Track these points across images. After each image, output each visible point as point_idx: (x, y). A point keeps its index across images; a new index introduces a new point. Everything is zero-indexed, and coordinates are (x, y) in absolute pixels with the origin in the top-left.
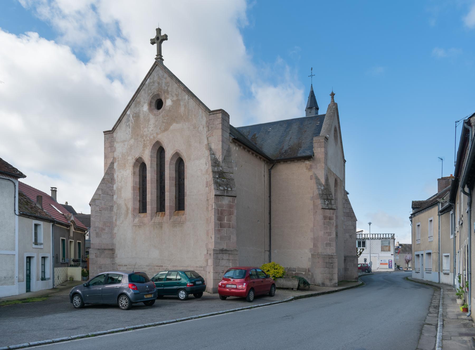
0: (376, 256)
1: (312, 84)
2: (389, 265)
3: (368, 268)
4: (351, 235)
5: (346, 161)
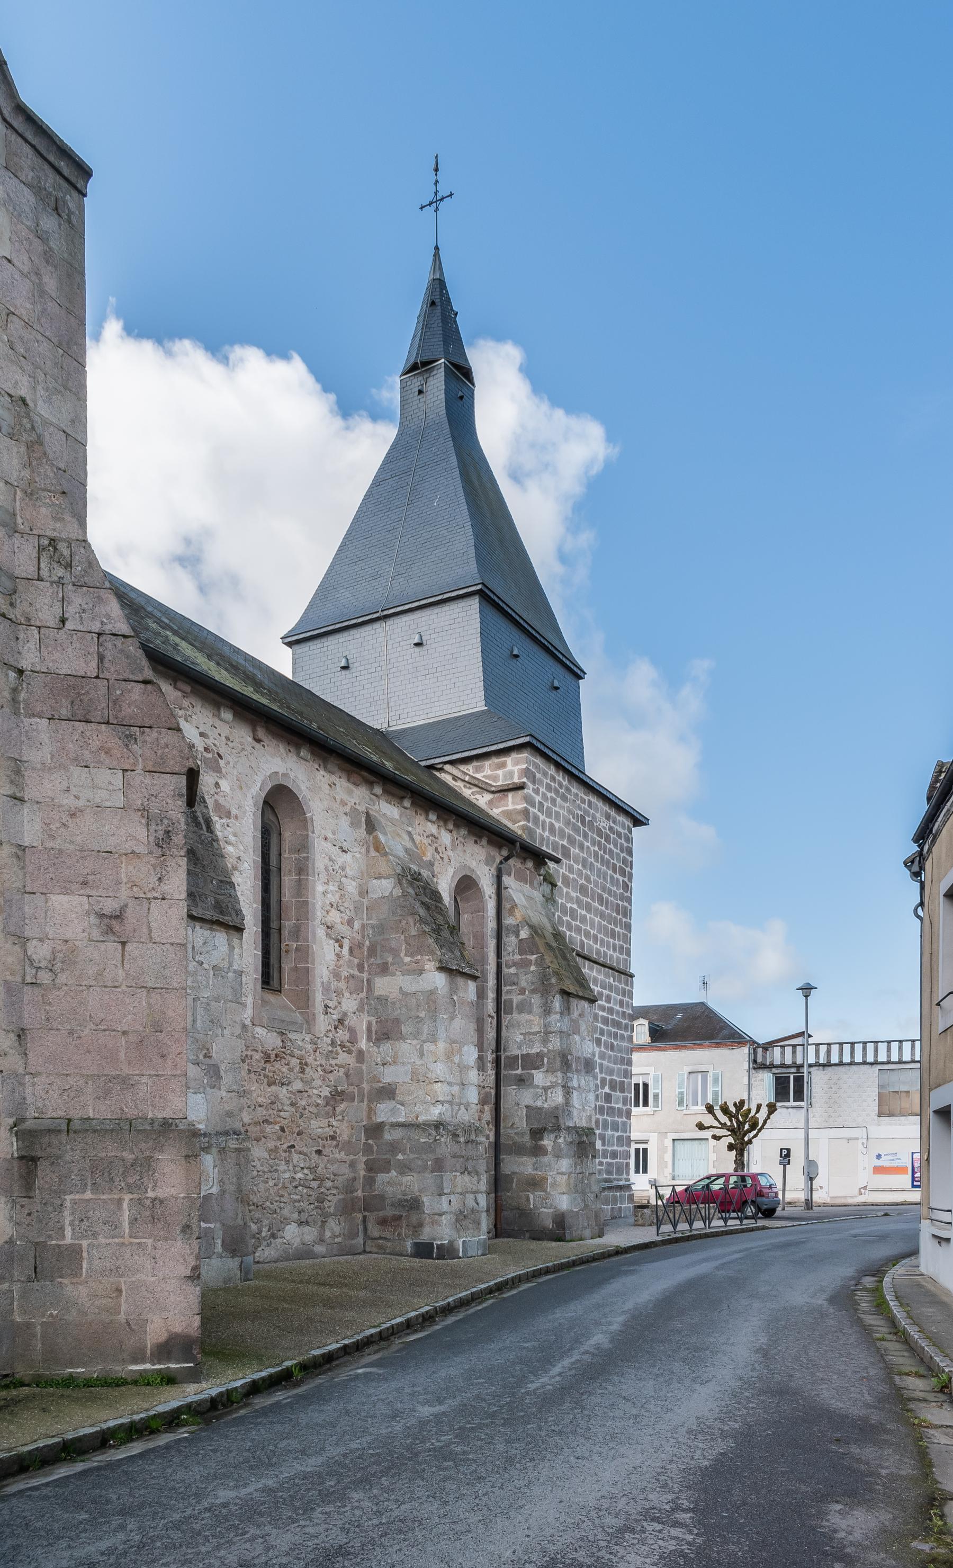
0: (857, 1139)
1: (437, 248)
2: (913, 1173)
3: (760, 1194)
4: (110, 906)
5: (85, 172)
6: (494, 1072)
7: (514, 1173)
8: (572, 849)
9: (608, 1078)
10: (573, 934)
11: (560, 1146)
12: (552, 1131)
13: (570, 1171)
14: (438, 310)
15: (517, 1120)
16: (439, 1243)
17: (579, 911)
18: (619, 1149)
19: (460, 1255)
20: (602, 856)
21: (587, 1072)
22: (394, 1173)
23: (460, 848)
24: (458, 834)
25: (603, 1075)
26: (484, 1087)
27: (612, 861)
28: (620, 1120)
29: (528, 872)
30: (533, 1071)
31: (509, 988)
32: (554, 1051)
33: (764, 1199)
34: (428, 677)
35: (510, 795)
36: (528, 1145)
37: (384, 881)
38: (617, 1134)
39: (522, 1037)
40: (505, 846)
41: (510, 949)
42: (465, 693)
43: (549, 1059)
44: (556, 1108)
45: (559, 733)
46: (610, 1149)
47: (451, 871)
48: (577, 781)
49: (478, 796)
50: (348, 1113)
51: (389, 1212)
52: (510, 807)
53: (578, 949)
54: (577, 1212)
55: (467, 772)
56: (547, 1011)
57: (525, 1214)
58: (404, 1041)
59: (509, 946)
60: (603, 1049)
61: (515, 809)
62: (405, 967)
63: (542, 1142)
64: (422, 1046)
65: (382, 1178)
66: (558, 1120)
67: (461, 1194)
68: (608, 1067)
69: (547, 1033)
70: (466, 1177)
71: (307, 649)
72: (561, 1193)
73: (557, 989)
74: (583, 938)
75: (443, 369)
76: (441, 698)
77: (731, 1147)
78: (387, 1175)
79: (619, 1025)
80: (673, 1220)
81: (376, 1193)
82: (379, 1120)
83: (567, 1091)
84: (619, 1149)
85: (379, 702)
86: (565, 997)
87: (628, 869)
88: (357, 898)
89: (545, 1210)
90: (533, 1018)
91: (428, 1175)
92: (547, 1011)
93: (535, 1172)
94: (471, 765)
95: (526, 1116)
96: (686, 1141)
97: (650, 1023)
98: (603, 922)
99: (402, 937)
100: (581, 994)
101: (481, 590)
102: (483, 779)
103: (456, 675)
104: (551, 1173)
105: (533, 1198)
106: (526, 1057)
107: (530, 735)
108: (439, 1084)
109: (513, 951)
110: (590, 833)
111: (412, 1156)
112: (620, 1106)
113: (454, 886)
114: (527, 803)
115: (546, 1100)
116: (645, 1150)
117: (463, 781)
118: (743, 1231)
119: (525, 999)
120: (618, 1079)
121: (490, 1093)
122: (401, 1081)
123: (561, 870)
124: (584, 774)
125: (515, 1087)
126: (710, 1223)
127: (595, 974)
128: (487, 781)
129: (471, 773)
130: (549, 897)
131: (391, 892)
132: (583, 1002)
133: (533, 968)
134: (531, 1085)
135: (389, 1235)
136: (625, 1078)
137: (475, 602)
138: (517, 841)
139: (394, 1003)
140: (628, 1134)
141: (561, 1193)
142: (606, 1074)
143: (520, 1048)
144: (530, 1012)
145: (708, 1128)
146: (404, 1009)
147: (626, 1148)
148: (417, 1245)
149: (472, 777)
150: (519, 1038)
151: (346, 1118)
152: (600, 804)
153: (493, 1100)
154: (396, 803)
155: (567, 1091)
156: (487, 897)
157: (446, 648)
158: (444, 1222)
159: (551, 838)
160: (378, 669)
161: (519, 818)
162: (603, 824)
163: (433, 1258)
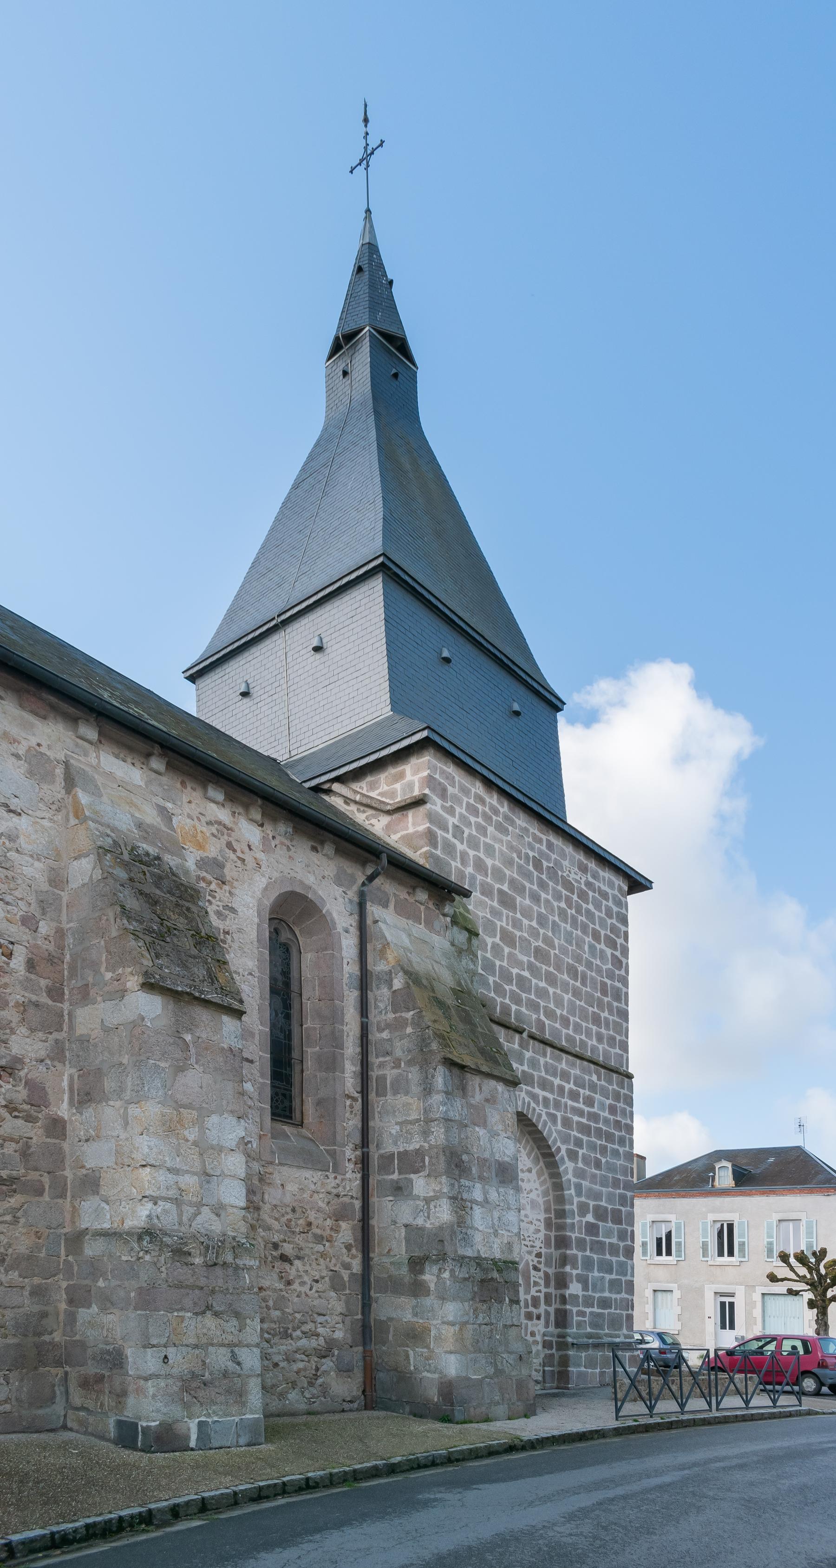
1: (368, 211)
6: (359, 1176)
7: (391, 1319)
8: (519, 899)
9: (592, 1203)
10: (523, 1010)
11: (445, 1283)
12: (436, 1262)
13: (465, 1318)
14: (366, 275)
15: (394, 1244)
16: (144, 1424)
17: (534, 981)
18: (614, 1296)
19: (193, 1444)
20: (573, 916)
21: (503, 1182)
22: (95, 1308)
23: (281, 852)
24: (276, 830)
25: (583, 1199)
26: (338, 1196)
27: (592, 926)
28: (614, 1259)
29: (422, 908)
30: (412, 1176)
31: (381, 1059)
32: (436, 1147)
33: (827, 1371)
34: (329, 688)
35: (410, 814)
36: (407, 1279)
37: (84, 861)
38: (608, 1277)
39: (398, 1127)
40: (371, 861)
41: (382, 1005)
42: (369, 699)
43: (431, 1158)
44: (441, 1228)
45: (522, 770)
46: (597, 1295)
47: (261, 882)
48: (525, 812)
49: (374, 821)
50: (25, 1212)
51: (91, 1369)
52: (411, 830)
53: (534, 1030)
54: (481, 1381)
55: (360, 791)
56: (427, 1090)
57: (404, 1378)
58: (107, 1102)
59: (381, 1001)
60: (580, 1165)
61: (417, 832)
62: (106, 989)
63: (424, 1277)
64: (126, 1109)
65: (83, 1314)
66: (443, 1246)
67: (196, 1346)
68: (590, 1190)
69: (428, 1121)
70: (209, 1321)
71: (209, 681)
72: (446, 1352)
73: (439, 1057)
74: (542, 1017)
75: (368, 339)
76: (344, 711)
77: (811, 1304)
78: (88, 1311)
79: (610, 1137)
80: (678, 1395)
81: (77, 1337)
82: (83, 1227)
83: (460, 1204)
84: (614, 1296)
85: (280, 730)
86: (456, 1071)
87: (620, 941)
88: (45, 887)
89: (429, 1375)
90: (411, 1101)
91: (133, 1314)
92: (427, 1090)
93: (415, 1319)
94: (365, 782)
95: (405, 1238)
96: (777, 1297)
97: (733, 1165)
98: (578, 1002)
99: (103, 943)
100: (484, 1068)
101: (382, 564)
102: (379, 798)
103: (360, 679)
104: (435, 1322)
105: (414, 1356)
106: (403, 1155)
107: (428, 727)
108: (148, 1169)
109: (386, 1008)
110: (551, 884)
111: (114, 1283)
112: (614, 1240)
113: (268, 903)
114: (431, 822)
115: (428, 1217)
116: (732, 1305)
117: (356, 802)
118: (773, 1416)
119: (400, 1074)
120: (610, 1207)
121: (352, 1205)
122: (105, 1165)
123: (499, 923)
124: (565, 823)
125: (391, 1198)
126: (718, 1404)
127: (564, 1065)
128: (384, 799)
129: (364, 792)
130: (465, 947)
131: (91, 876)
132: (493, 1083)
133: (409, 1030)
134: (410, 1196)
135: (90, 1404)
136: (622, 1205)
137: (377, 585)
138: (381, 852)
139: (95, 1046)
140: (629, 1278)
141: (446, 1352)
142: (588, 1197)
143: (395, 1143)
144: (407, 1093)
145: (782, 1280)
146: (106, 1054)
147: (626, 1296)
148: (120, 1424)
149: (363, 795)
150: (395, 1130)
151: (22, 1220)
152: (569, 849)
153: (358, 1215)
154: (138, 764)
155: (460, 1204)
156: (339, 929)
157: (348, 647)
158: (151, 1391)
159: (479, 877)
160: (278, 689)
161: (422, 842)
162: (574, 876)
163: (135, 1448)
